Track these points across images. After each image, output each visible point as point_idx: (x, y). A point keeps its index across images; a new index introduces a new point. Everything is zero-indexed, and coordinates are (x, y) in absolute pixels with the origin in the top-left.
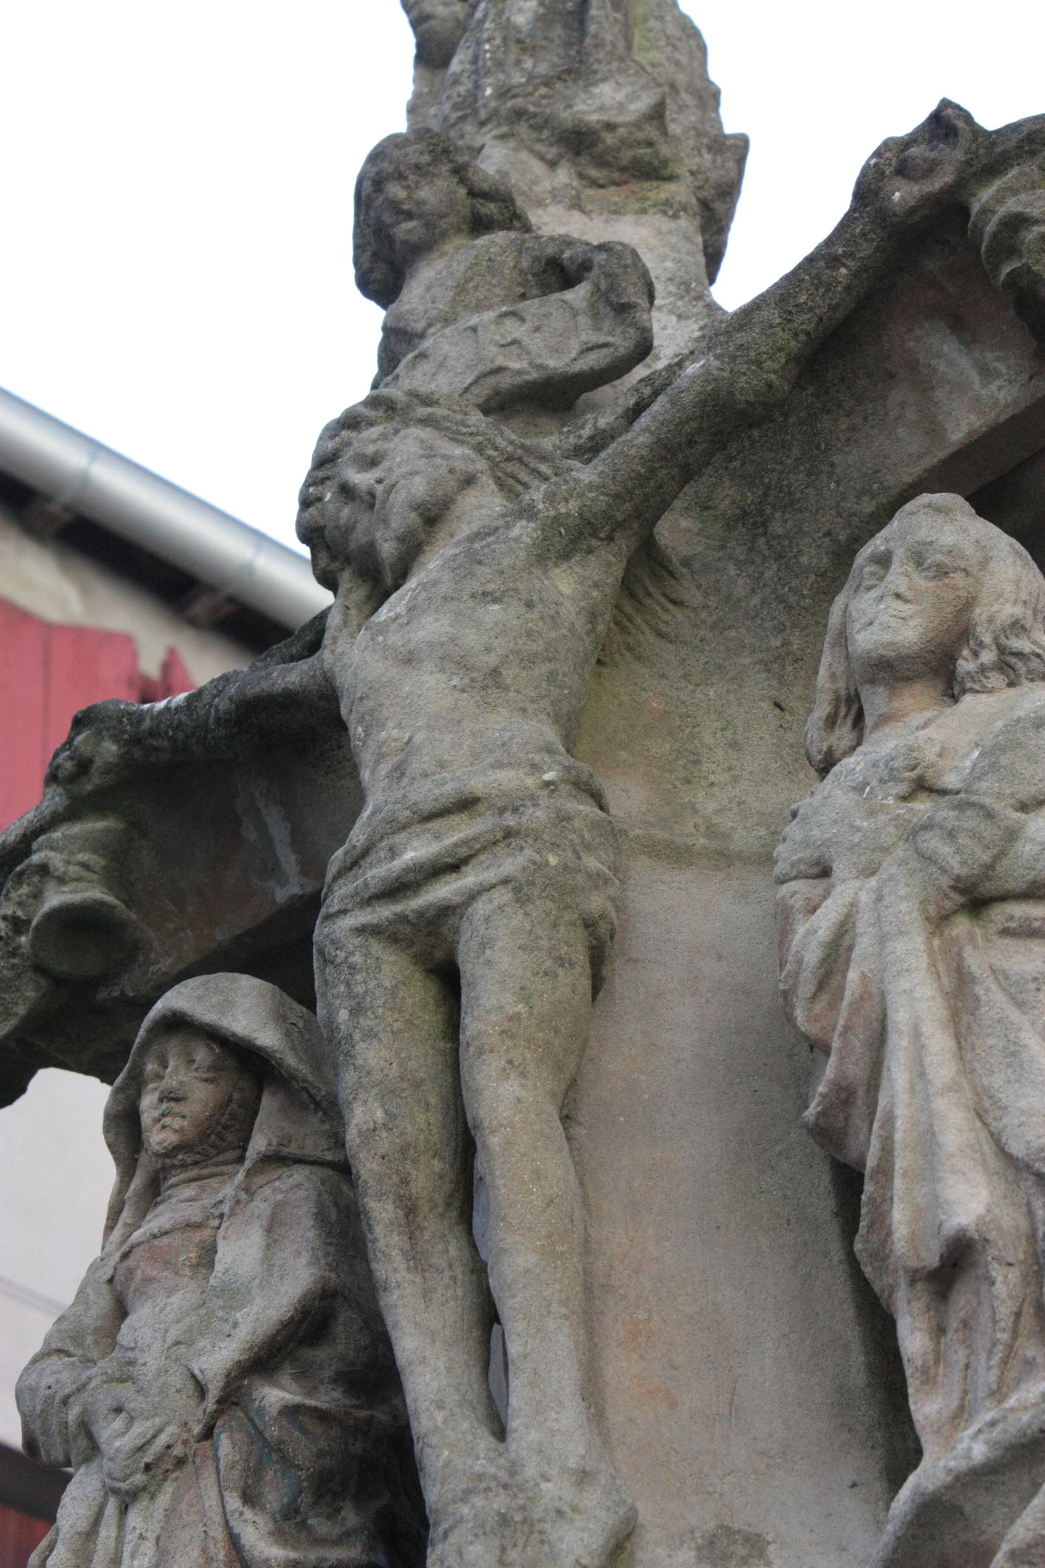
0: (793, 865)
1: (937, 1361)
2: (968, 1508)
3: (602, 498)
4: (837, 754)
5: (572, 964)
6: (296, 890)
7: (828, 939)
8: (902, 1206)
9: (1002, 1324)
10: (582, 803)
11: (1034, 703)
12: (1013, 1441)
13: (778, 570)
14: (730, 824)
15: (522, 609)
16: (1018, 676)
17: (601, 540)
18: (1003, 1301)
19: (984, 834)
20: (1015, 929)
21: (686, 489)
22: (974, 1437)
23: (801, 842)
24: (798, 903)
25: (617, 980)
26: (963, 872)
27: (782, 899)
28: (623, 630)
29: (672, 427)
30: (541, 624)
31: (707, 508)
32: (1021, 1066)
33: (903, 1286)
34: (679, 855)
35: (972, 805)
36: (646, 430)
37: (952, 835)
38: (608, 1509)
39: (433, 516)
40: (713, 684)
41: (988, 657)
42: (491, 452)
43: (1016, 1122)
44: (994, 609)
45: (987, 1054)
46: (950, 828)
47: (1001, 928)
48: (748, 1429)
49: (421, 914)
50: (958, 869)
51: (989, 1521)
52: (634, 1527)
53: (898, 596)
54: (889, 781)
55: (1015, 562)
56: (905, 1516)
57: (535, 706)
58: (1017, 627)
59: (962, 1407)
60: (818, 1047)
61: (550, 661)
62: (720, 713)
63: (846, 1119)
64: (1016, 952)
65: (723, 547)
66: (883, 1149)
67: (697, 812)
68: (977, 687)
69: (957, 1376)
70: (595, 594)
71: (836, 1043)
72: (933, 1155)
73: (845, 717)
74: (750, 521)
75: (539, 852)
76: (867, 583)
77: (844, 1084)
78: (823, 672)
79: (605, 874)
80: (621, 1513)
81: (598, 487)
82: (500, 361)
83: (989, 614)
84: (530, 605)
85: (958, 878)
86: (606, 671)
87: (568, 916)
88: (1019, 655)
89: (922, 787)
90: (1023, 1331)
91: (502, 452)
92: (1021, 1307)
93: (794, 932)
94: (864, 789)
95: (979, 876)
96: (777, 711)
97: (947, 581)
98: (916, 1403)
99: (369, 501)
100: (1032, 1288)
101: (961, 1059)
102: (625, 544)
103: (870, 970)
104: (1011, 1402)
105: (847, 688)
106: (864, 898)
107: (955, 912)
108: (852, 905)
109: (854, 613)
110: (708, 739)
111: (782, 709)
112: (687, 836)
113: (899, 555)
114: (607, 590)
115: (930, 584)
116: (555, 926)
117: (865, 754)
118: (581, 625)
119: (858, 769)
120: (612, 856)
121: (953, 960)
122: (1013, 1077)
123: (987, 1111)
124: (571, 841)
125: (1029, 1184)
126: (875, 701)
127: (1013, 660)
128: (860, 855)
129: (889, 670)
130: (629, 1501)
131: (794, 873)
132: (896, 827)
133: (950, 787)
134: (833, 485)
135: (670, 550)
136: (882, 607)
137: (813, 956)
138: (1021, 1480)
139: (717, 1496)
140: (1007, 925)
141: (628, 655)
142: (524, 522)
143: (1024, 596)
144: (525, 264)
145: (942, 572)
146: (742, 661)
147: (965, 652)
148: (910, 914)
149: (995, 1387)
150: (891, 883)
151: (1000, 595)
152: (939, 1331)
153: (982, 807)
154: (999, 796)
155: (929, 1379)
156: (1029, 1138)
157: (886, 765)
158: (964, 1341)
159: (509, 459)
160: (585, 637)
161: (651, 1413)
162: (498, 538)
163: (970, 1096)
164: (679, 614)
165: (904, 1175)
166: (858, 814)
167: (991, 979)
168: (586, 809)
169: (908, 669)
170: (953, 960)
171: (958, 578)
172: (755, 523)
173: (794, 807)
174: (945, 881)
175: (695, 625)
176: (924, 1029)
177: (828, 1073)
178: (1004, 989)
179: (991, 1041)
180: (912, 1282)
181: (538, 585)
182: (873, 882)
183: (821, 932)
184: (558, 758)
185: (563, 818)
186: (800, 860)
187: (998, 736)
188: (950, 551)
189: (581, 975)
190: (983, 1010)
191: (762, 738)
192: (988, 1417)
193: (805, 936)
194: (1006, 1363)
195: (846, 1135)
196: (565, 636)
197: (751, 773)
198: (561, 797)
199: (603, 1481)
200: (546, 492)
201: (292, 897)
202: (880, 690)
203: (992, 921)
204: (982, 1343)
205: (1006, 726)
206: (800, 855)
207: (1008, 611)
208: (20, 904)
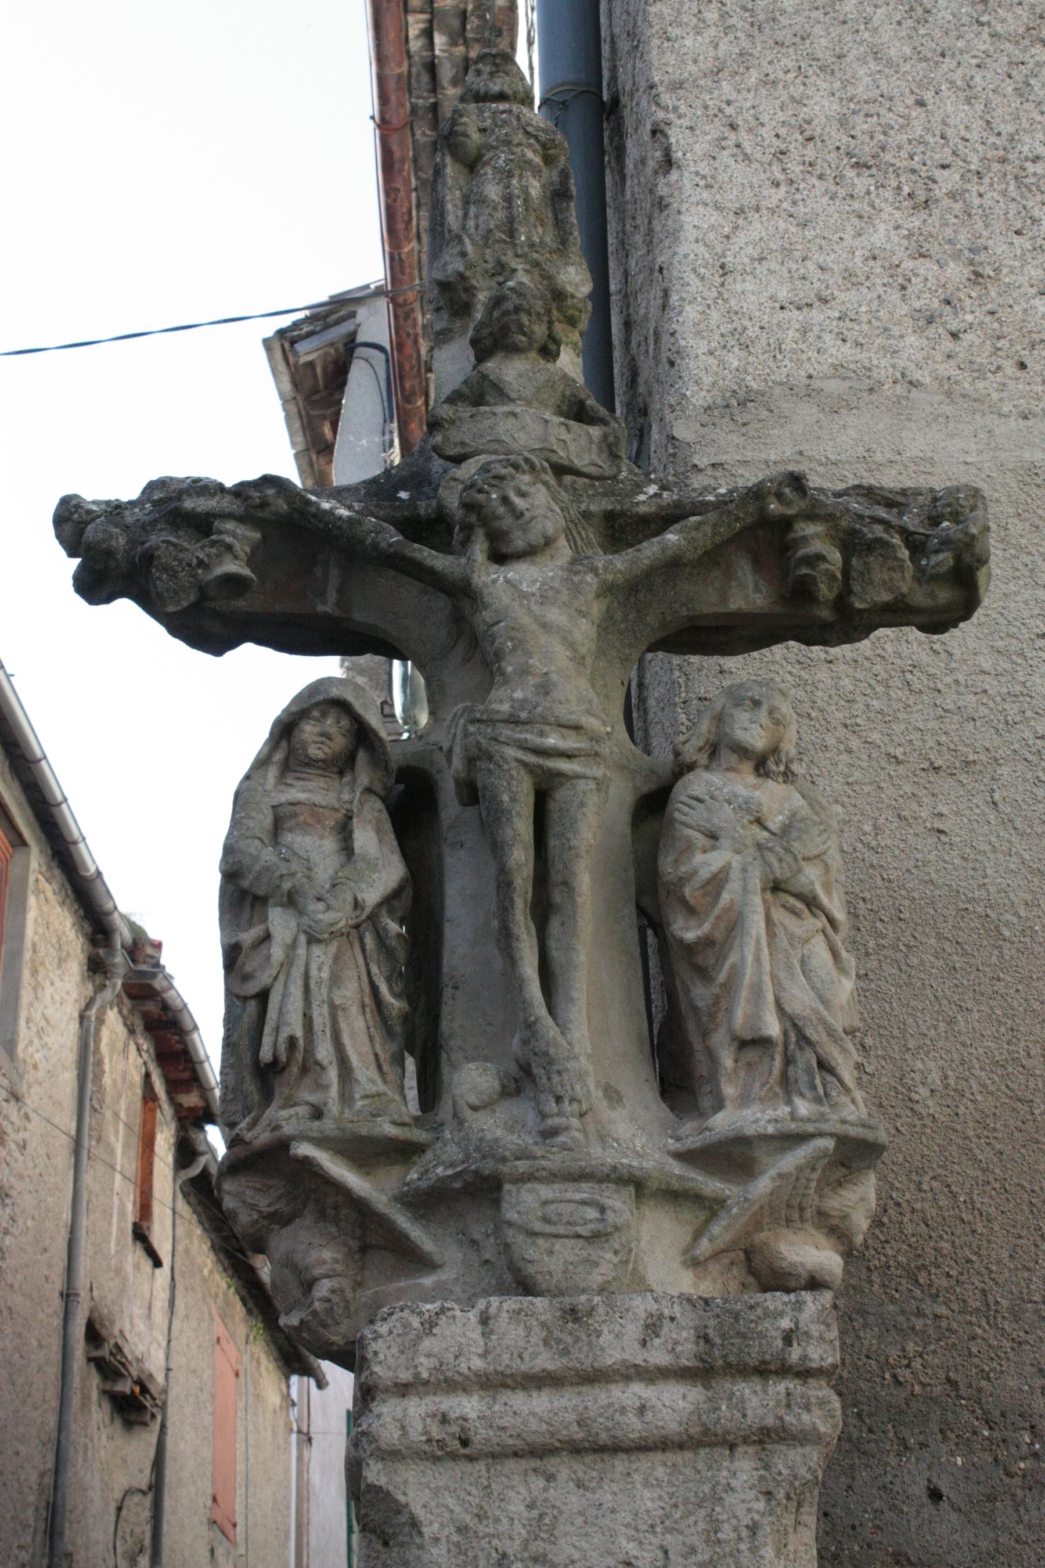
6: (329, 610)
37: (780, 860)
49: (550, 770)
82: (555, 447)
99: (519, 515)
129: (742, 751)
144: (567, 393)
174: (771, 877)
201: (325, 613)
208: (208, 556)
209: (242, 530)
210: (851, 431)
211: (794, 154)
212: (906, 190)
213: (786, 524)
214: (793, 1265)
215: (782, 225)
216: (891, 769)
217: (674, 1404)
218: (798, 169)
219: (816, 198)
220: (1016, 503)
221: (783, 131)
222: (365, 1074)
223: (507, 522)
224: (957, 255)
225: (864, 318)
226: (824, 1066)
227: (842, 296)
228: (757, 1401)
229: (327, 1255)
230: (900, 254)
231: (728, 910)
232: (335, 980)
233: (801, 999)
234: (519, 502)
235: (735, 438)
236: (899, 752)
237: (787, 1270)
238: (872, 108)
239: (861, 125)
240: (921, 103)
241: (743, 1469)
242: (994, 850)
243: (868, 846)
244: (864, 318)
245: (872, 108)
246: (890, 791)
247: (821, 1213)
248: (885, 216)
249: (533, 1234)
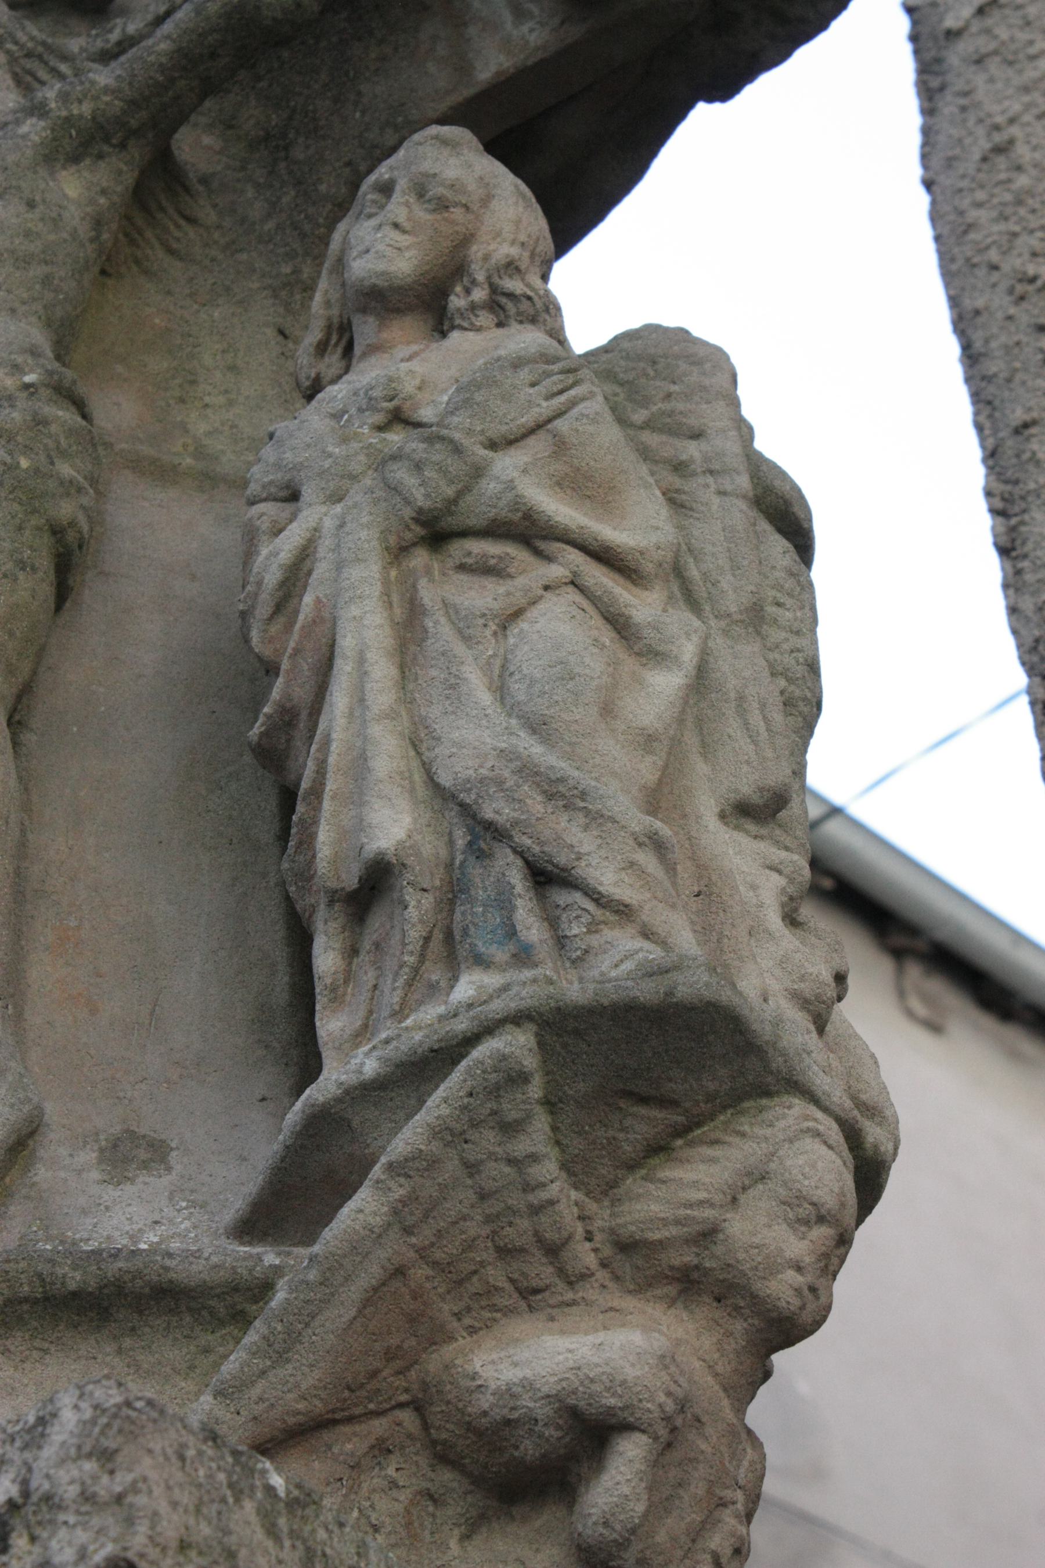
0: (264, 487)
1: (346, 982)
2: (355, 1123)
3: (116, 102)
4: (324, 381)
5: (34, 569)
7: (288, 562)
8: (327, 828)
9: (410, 948)
10: (62, 409)
11: (518, 344)
12: (404, 1058)
13: (297, 196)
14: (220, 447)
15: (22, 208)
16: (507, 317)
17: (114, 146)
18: (414, 925)
19: (451, 469)
20: (471, 565)
21: (207, 104)
22: (367, 1054)
23: (274, 465)
24: (265, 524)
25: (87, 592)
26: (427, 504)
27: (250, 520)
28: (132, 242)
29: (194, 37)
30: (40, 225)
31: (231, 127)
32: (459, 699)
33: (322, 906)
34: (163, 473)
35: (442, 439)
36: (168, 37)
37: (418, 467)
38: (12, 1106)
40: (218, 305)
41: (479, 295)
42: (10, 46)
43: (447, 752)
44: (491, 248)
45: (428, 685)
46: (417, 460)
47: (458, 563)
48: (166, 1040)
50: (420, 498)
51: (375, 1135)
52: (38, 1125)
53: (396, 226)
54: (367, 410)
55: (517, 203)
56: (295, 1126)
57: (24, 308)
58: (511, 267)
59: (366, 1026)
60: (271, 669)
61: (46, 263)
62: (223, 335)
63: (288, 741)
64: (470, 588)
65: (243, 168)
66: (318, 772)
67: (187, 432)
68: (465, 324)
69: (365, 995)
70: (102, 201)
71: (285, 665)
72: (363, 779)
73: (336, 345)
74: (273, 144)
75: (10, 453)
76: (368, 210)
77: (288, 705)
78: (318, 297)
79: (79, 482)
80: (25, 1111)
81: (113, 92)
83: (485, 252)
84: (31, 205)
85: (420, 511)
86: (110, 282)
87: (35, 521)
88: (511, 296)
89: (398, 418)
90: (430, 955)
91: (22, 46)
92: (431, 932)
93: (258, 553)
94: (342, 416)
95: (441, 510)
96: (280, 338)
97: (446, 215)
98: (322, 1019)
100: (444, 914)
101: (403, 688)
102: (138, 152)
103: (326, 595)
104: (409, 1022)
105: (341, 316)
106: (328, 523)
107: (414, 544)
108: (315, 530)
109: (352, 240)
110: (208, 360)
111: (285, 337)
112: (175, 454)
113: (402, 184)
114: (115, 198)
115: (429, 217)
116: (20, 528)
117: (349, 383)
118: (85, 231)
119: (339, 396)
120: (90, 467)
121: (407, 591)
122: (450, 709)
123: (422, 741)
124: (45, 445)
125: (453, 813)
126: (365, 329)
127: (503, 300)
128: (328, 481)
129: (382, 300)
130: (36, 1099)
131: (264, 495)
132: (367, 455)
133: (425, 420)
134: (358, 115)
135: (188, 167)
136: (379, 235)
137: (272, 577)
138: (408, 1097)
139: (127, 1102)
140: (464, 561)
141: (135, 268)
142: (34, 120)
143: (522, 238)
145: (442, 205)
146: (251, 285)
147: (458, 289)
148: (369, 542)
149: (397, 1008)
150: (355, 511)
151: (498, 234)
152: (353, 952)
153: (451, 441)
154: (470, 432)
155: (337, 998)
156: (457, 769)
157: (366, 393)
158: (375, 963)
159: (29, 55)
160: (87, 244)
161: (70, 1018)
162: (6, 134)
163: (407, 724)
164: (191, 232)
165: (333, 798)
166: (331, 440)
167: (441, 612)
168: (65, 415)
169: (399, 301)
170: (407, 591)
171: (457, 213)
172: (277, 147)
173: (271, 429)
174: (408, 513)
175: (207, 245)
176: (369, 655)
177: (274, 694)
178: (453, 623)
179: (434, 673)
180: (331, 903)
181: (42, 186)
182: (338, 508)
183: (282, 555)
184: (42, 361)
185: (40, 422)
186: (271, 482)
187: (475, 373)
188: (453, 186)
189: (43, 580)
190: (429, 642)
191: (261, 364)
192: (383, 1035)
193: (267, 558)
194: (410, 986)
195: (287, 757)
196: (65, 241)
197: (247, 397)
198: (40, 400)
199: (10, 1079)
200: (60, 91)
202: (371, 319)
203: (450, 556)
204: (390, 964)
205: (485, 364)
206: (271, 477)
207: (504, 251)
214: (509, 1393)
231: (316, 621)
233: (475, 739)
237: (497, 1414)
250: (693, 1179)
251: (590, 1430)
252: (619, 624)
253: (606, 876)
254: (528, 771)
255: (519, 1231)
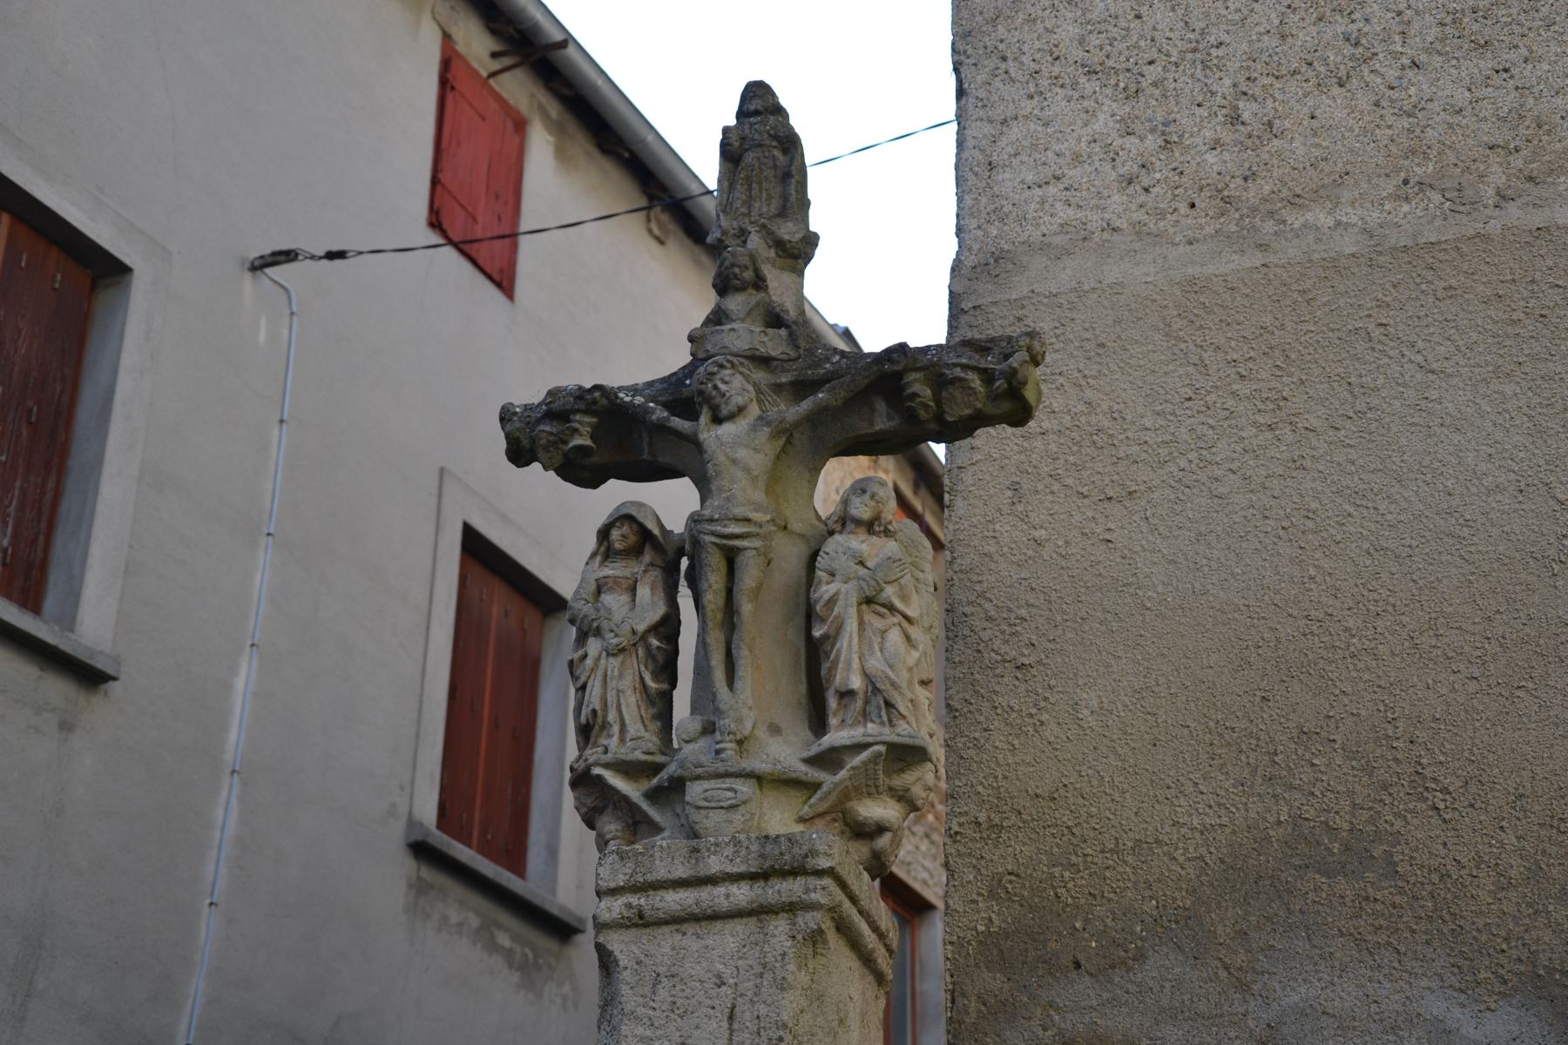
39: (741, 410)
129: (858, 522)
209: (587, 419)
210: (1068, 271)
211: (1045, 73)
212: (1122, 85)
213: (899, 375)
215: (1032, 126)
216: (1079, 502)
217: (742, 894)
218: (1046, 83)
219: (1059, 102)
220: (1177, 307)
221: (1038, 56)
222: (634, 728)
223: (718, 400)
224: (1153, 130)
225: (1084, 187)
226: (889, 705)
227: (1071, 173)
228: (791, 889)
229: (613, 827)
230: (1114, 135)
231: (838, 617)
232: (621, 675)
233: (876, 663)
234: (723, 387)
235: (989, 286)
236: (1085, 490)
238: (1102, 27)
239: (1094, 40)
240: (1138, 17)
241: (779, 926)
242: (1144, 550)
243: (1059, 554)
244: (1084, 187)
245: (1102, 27)
246: (1078, 517)
247: (891, 789)
248: (1105, 108)
249: (699, 808)
250: (908, 778)
251: (880, 829)
252: (908, 638)
253: (902, 709)
254: (887, 677)
255: (871, 782)
